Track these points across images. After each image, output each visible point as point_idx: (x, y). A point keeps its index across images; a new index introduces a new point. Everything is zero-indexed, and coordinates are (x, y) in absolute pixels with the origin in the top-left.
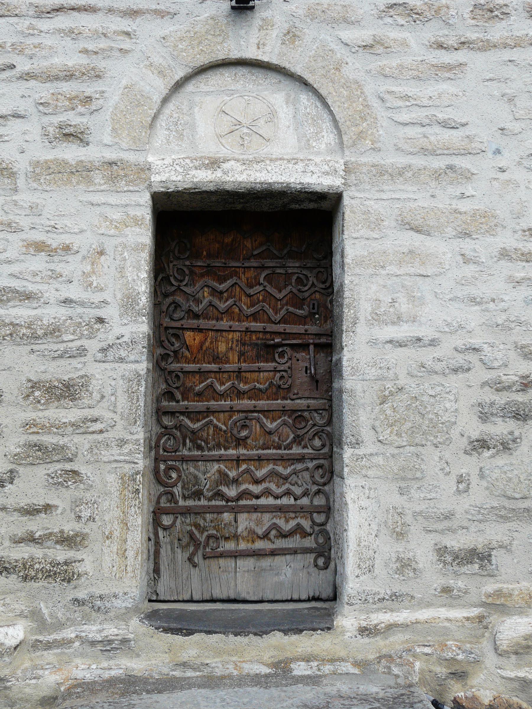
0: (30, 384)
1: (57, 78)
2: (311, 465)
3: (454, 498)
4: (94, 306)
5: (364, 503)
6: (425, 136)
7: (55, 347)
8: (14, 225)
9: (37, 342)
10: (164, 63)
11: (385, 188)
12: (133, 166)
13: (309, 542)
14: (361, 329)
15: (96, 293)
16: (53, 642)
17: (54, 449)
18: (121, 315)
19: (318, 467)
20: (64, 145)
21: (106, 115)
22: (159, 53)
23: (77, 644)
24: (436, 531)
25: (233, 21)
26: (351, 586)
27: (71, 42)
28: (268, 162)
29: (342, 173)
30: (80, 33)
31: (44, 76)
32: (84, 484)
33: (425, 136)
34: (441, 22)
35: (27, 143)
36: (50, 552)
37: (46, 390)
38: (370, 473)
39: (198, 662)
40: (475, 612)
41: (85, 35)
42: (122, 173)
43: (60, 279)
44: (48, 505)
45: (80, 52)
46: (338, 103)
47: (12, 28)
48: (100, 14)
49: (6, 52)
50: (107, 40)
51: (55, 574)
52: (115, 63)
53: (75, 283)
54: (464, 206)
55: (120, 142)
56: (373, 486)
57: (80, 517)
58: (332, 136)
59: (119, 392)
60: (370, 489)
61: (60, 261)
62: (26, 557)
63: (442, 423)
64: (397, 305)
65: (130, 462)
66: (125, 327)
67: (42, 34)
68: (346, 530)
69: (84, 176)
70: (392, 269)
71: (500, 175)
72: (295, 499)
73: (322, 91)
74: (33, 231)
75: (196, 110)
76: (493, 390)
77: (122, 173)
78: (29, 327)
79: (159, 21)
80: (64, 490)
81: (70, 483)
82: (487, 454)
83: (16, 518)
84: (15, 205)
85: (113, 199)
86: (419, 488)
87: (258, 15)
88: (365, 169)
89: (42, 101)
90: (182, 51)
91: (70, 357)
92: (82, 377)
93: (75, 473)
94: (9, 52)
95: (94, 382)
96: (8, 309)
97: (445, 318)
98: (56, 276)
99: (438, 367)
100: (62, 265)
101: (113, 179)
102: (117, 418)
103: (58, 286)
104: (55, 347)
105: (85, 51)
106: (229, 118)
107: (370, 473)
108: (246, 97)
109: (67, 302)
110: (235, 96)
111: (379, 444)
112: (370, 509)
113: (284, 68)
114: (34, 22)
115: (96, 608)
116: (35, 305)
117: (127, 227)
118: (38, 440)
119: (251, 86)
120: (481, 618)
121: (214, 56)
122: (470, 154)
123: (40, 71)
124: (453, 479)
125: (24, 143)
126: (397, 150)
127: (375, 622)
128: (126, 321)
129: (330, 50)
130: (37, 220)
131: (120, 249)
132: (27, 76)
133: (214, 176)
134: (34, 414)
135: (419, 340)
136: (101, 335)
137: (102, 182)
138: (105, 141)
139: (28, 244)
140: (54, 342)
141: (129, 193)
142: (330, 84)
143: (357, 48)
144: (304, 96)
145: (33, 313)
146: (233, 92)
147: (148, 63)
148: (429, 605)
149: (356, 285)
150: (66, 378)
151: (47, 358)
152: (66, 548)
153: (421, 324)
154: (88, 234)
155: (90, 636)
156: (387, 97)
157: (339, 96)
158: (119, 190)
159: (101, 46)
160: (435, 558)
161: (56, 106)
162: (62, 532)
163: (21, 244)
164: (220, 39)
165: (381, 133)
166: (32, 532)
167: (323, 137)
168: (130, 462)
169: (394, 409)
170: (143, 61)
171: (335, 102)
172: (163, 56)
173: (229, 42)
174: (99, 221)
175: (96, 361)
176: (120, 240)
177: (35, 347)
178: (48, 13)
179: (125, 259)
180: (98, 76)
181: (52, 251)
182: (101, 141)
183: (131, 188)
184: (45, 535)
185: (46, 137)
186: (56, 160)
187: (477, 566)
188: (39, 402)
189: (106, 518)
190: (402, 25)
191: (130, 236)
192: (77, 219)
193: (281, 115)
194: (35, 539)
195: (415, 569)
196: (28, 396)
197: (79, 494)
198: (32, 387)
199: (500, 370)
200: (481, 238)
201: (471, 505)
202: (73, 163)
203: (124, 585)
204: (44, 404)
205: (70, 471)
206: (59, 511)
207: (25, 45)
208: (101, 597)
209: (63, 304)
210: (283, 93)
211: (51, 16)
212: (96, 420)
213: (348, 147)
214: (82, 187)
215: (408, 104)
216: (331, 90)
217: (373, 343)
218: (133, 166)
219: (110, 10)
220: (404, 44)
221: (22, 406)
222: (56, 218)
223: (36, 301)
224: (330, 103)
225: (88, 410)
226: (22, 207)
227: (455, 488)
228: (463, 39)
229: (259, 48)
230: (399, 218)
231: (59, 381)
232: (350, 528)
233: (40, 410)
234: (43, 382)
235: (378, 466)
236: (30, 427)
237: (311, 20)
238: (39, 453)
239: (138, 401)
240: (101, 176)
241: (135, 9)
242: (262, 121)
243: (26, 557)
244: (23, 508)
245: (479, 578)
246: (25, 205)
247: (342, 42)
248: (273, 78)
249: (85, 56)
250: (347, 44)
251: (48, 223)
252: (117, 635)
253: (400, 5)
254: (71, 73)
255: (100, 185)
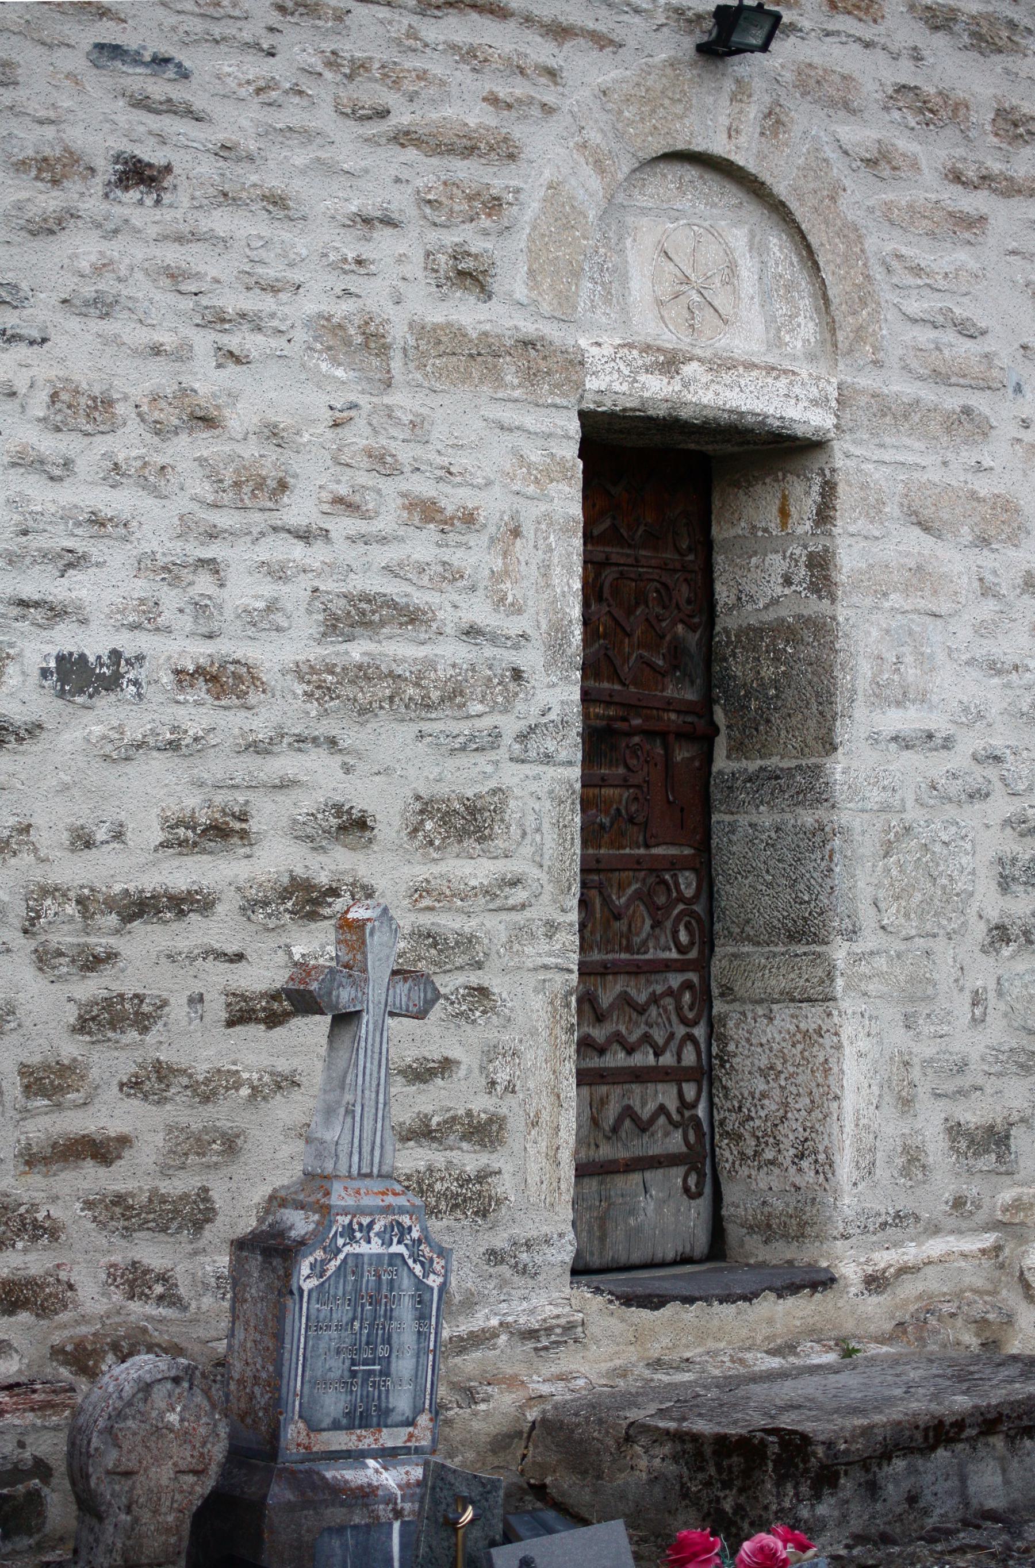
0: (418, 806)
1: (451, 150)
2: (675, 980)
3: (969, 1033)
4: (509, 643)
5: (863, 1044)
6: (938, 348)
7: (454, 727)
8: (389, 459)
9: (429, 715)
10: (603, 145)
11: (887, 440)
12: (558, 354)
13: (675, 1142)
14: (860, 711)
15: (511, 618)
16: (468, 1339)
17: (457, 943)
18: (547, 666)
19: (687, 985)
20: (458, 294)
21: (520, 240)
22: (596, 121)
23: (503, 1338)
24: (946, 1096)
25: (699, 75)
26: (846, 1202)
27: (470, 74)
28: (741, 369)
29: (834, 404)
30: (486, 60)
31: (433, 142)
32: (498, 1014)
33: (938, 348)
34: (958, 132)
35: (405, 283)
36: (455, 1155)
37: (441, 819)
38: (872, 987)
39: (676, 1356)
40: (989, 1239)
41: (494, 66)
42: (543, 366)
43: (460, 584)
44: (446, 1059)
45: (484, 99)
46: (832, 267)
47: (381, 30)
48: (512, 24)
49: (370, 79)
50: (526, 82)
51: (464, 1201)
52: (532, 130)
53: (480, 592)
54: (983, 487)
55: (540, 299)
56: (875, 1013)
57: (493, 1083)
58: (811, 325)
59: (546, 827)
60: (870, 1018)
61: (459, 545)
62: (422, 1169)
63: (958, 895)
64: (902, 668)
65: (562, 969)
66: (552, 691)
67: (427, 50)
68: (837, 1098)
69: (490, 366)
70: (896, 599)
71: (1023, 434)
72: (657, 1055)
73: (812, 239)
74: (416, 476)
75: (629, 242)
76: (1016, 834)
77: (543, 366)
78: (417, 685)
79: (595, 54)
80: (468, 1028)
81: (478, 1014)
82: (1007, 951)
83: (399, 1089)
84: (389, 416)
85: (529, 421)
86: (929, 1016)
87: (730, 70)
88: (863, 401)
89: (430, 197)
90: (630, 123)
91: (477, 750)
92: (494, 792)
93: (483, 992)
94: (376, 81)
95: (512, 803)
96: (380, 642)
97: (960, 696)
98: (451, 575)
99: (954, 788)
100: (460, 553)
101: (531, 376)
102: (544, 877)
103: (455, 597)
104: (454, 727)
105: (493, 100)
106: (671, 265)
107: (872, 987)
108: (696, 228)
109: (472, 632)
110: (682, 222)
111: (881, 932)
112: (870, 1056)
113: (763, 183)
114: (415, 20)
115: (521, 1266)
116: (423, 636)
117: (552, 481)
118: (433, 924)
119: (702, 206)
120: (998, 1249)
121: (671, 142)
122: (989, 388)
123: (426, 131)
124: (967, 997)
125: (401, 284)
126: (903, 368)
127: (882, 1265)
128: (554, 679)
129: (825, 160)
130: (419, 451)
131: (543, 527)
132: (404, 138)
133: (671, 389)
134: (425, 868)
135: (930, 736)
136: (520, 706)
137: (516, 381)
138: (517, 296)
139: (411, 504)
140: (455, 718)
141: (554, 410)
142: (823, 227)
143: (859, 163)
144: (775, 241)
145: (421, 652)
146: (677, 214)
147: (580, 140)
148: (935, 1230)
149: (853, 626)
150: (470, 794)
151: (443, 749)
152: (477, 1148)
153: (931, 708)
154: (497, 488)
155: (521, 1321)
156: (895, 264)
157: (833, 253)
158: (541, 402)
159: (518, 92)
160: (947, 1144)
161: (451, 210)
162: (469, 1114)
163: (400, 501)
164: (679, 109)
165: (884, 332)
166: (426, 1116)
167: (799, 326)
168: (562, 969)
169: (901, 866)
170: (573, 135)
171: (828, 262)
172: (602, 130)
173: (692, 117)
174: (513, 465)
175: (511, 759)
176: (543, 507)
177: (427, 727)
178: (438, 7)
179: (550, 550)
180: (512, 157)
181: (446, 523)
182: (510, 294)
183: (558, 401)
184: (446, 1122)
185: (434, 275)
186: (449, 325)
187: (993, 1156)
188: (431, 843)
189: (531, 1084)
190: (913, 129)
191: (556, 501)
192: (480, 456)
193: (744, 273)
194: (431, 1132)
195: (924, 1166)
196: (416, 830)
197: (492, 1036)
198: (422, 812)
199: (1023, 799)
200: (1002, 551)
201: (987, 1047)
202: (474, 336)
203: (556, 1218)
204: (439, 848)
205: (474, 989)
206: (462, 1072)
207: (402, 71)
208: (528, 1245)
209: (464, 637)
210: (745, 229)
211: (440, 14)
212: (515, 883)
213: (844, 355)
214: (486, 389)
215: (919, 282)
216: (825, 239)
217: (874, 739)
218: (558, 354)
219: (528, 20)
220: (915, 166)
221: (407, 851)
222: (450, 450)
223: (423, 628)
224: (821, 264)
225: (504, 861)
226: (399, 423)
227: (970, 1016)
228: (984, 172)
229: (730, 137)
230: (906, 502)
231: (461, 799)
232: (846, 1092)
233: (434, 860)
234: (437, 802)
235: (880, 974)
236: (421, 896)
237: (803, 95)
238: (433, 951)
239: (572, 844)
240: (513, 369)
241: (565, 24)
242: (717, 280)
243: (422, 1169)
244: (410, 1066)
245: (994, 1178)
246: (403, 417)
247: (841, 147)
248: (732, 194)
249: (492, 109)
250: (846, 153)
251: (440, 460)
252: (558, 1317)
253: (910, 89)
254: (474, 142)
255: (513, 388)
